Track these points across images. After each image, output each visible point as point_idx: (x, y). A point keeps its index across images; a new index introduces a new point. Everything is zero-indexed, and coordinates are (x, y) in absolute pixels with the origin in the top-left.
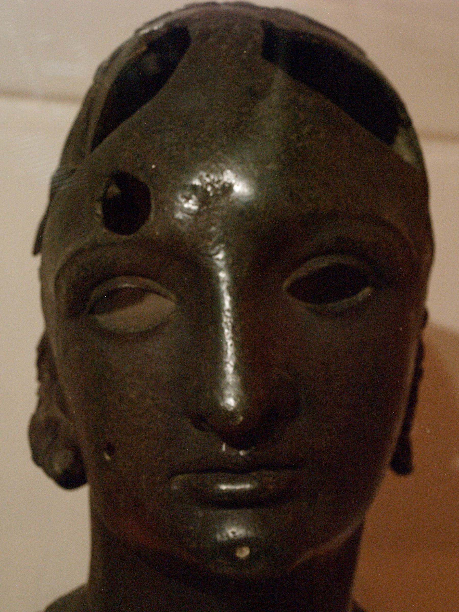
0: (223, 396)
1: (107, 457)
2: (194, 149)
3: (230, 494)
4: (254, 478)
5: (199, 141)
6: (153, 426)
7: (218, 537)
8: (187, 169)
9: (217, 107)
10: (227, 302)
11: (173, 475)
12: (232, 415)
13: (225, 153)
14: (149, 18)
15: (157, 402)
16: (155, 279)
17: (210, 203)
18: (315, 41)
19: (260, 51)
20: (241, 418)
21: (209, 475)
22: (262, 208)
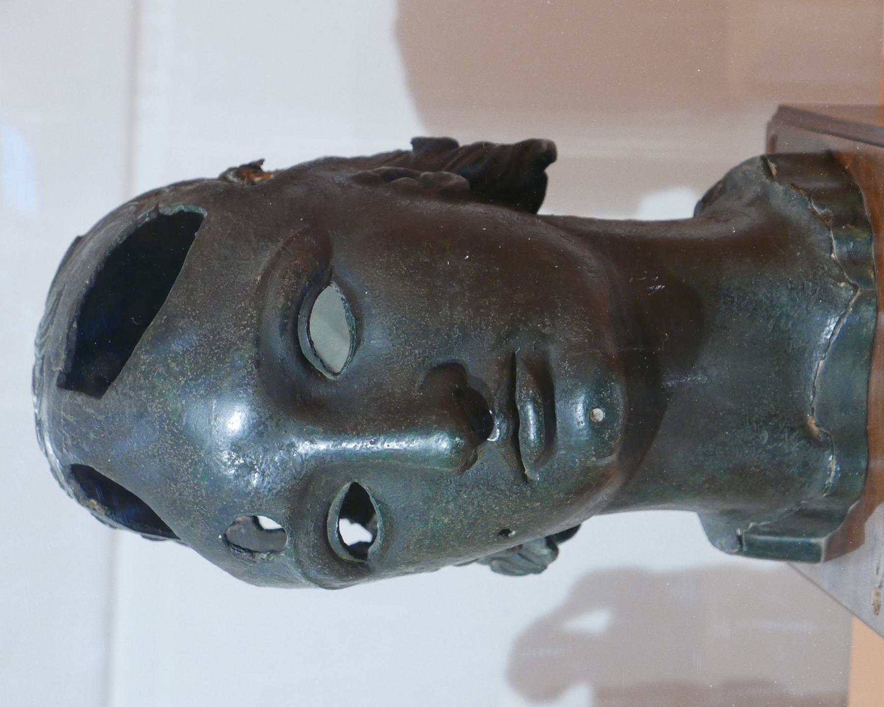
0: (439, 454)
1: (514, 533)
2: (199, 476)
3: (539, 431)
4: (522, 407)
5: (190, 470)
6: (476, 503)
7: (584, 439)
8: (218, 482)
9: (156, 450)
10: (350, 445)
11: (524, 478)
12: (455, 447)
13: (202, 448)
14: (41, 454)
15: (451, 499)
16: (330, 505)
17: (251, 463)
18: (75, 325)
19: (93, 400)
20: (457, 439)
21: (522, 449)
22: (255, 415)
